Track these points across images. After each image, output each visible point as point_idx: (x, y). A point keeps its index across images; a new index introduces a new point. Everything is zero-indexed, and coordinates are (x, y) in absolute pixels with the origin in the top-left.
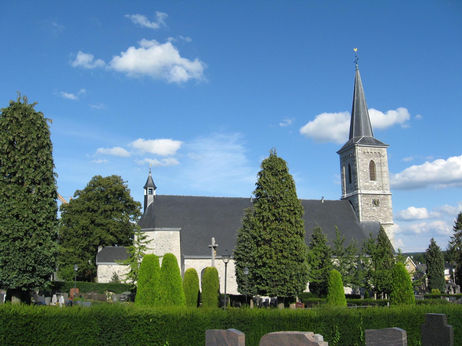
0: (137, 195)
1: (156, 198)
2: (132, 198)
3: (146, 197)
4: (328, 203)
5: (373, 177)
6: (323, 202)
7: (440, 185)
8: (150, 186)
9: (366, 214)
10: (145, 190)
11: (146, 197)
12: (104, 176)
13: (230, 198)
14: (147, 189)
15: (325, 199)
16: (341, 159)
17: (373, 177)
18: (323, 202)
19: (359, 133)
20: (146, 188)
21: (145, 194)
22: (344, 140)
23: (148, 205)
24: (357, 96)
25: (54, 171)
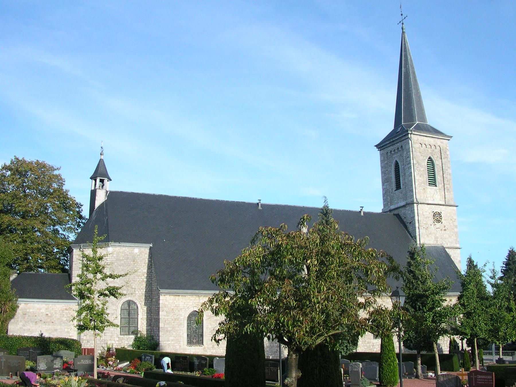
0: (79, 188)
1: (112, 196)
2: (67, 191)
3: (93, 194)
4: (368, 215)
5: (433, 182)
6: (362, 214)
7: (396, 206)
8: (100, 174)
9: (427, 235)
10: (94, 181)
11: (93, 194)
12: (28, 159)
13: (227, 202)
14: (96, 180)
15: (364, 210)
16: (381, 155)
17: (433, 182)
18: (362, 214)
19: (410, 118)
20: (94, 178)
21: (93, 188)
22: (388, 127)
23: (98, 204)
24: (406, 67)
25: (439, 342)
